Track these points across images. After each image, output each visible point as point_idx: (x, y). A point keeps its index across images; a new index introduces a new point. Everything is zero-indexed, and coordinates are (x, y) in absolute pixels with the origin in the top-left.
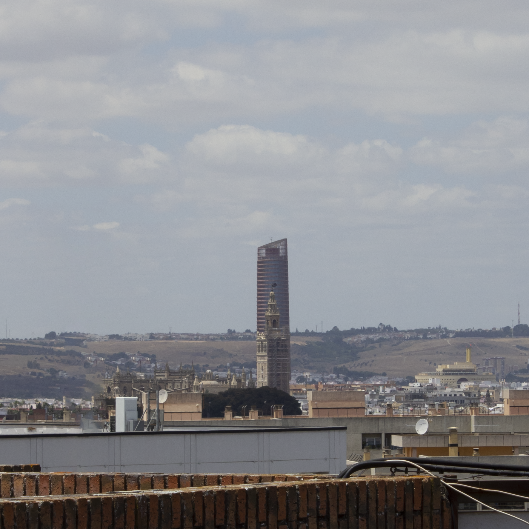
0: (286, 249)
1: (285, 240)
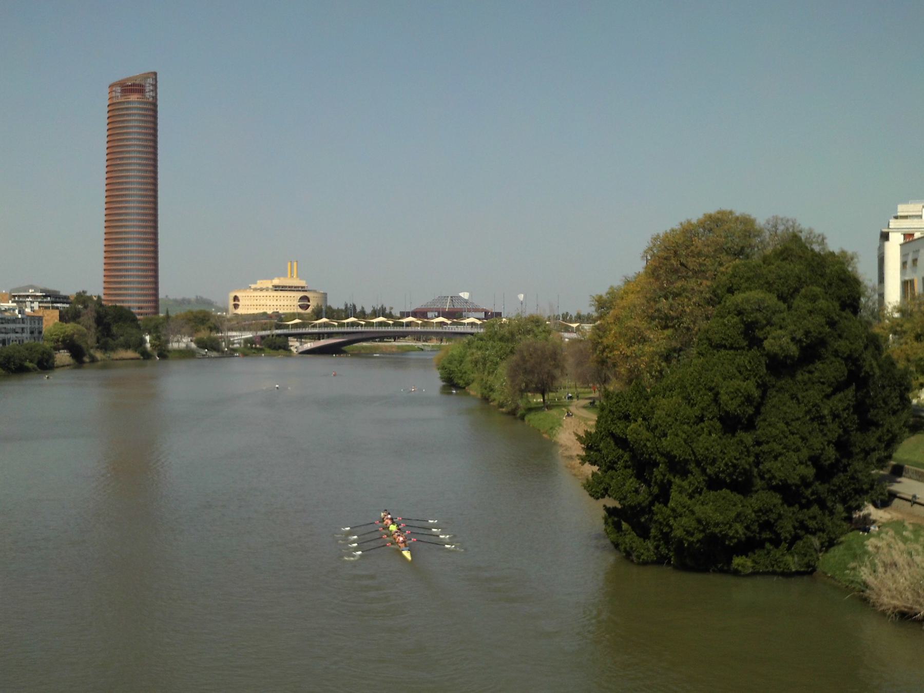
0: (155, 86)
1: (155, 74)
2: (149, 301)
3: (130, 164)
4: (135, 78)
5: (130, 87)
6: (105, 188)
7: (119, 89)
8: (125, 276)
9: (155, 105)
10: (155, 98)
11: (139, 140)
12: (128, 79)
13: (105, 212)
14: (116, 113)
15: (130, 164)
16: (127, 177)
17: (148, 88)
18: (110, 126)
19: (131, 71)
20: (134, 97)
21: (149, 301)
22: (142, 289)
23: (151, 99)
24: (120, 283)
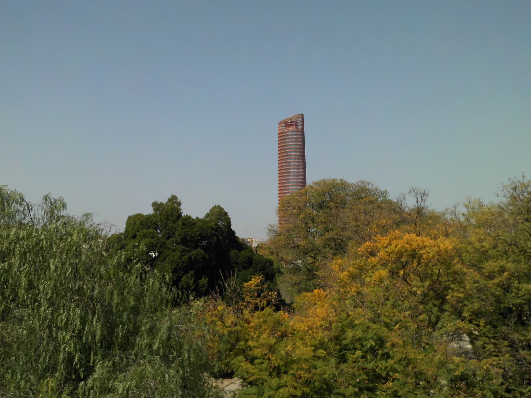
0: (303, 125)
1: (302, 115)
2: (299, 135)
3: (290, 165)
4: (291, 118)
5: (289, 123)
6: (278, 162)
7: (284, 125)
8: (288, 139)
9: (303, 132)
10: (303, 128)
11: (295, 158)
12: (288, 119)
13: (278, 189)
14: (282, 137)
15: (290, 165)
16: (289, 172)
17: (299, 123)
18: (280, 155)
19: (289, 114)
20: (291, 129)
21: (299, 135)
22: (296, 141)
23: (301, 129)
24: (285, 163)
